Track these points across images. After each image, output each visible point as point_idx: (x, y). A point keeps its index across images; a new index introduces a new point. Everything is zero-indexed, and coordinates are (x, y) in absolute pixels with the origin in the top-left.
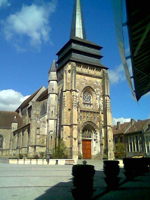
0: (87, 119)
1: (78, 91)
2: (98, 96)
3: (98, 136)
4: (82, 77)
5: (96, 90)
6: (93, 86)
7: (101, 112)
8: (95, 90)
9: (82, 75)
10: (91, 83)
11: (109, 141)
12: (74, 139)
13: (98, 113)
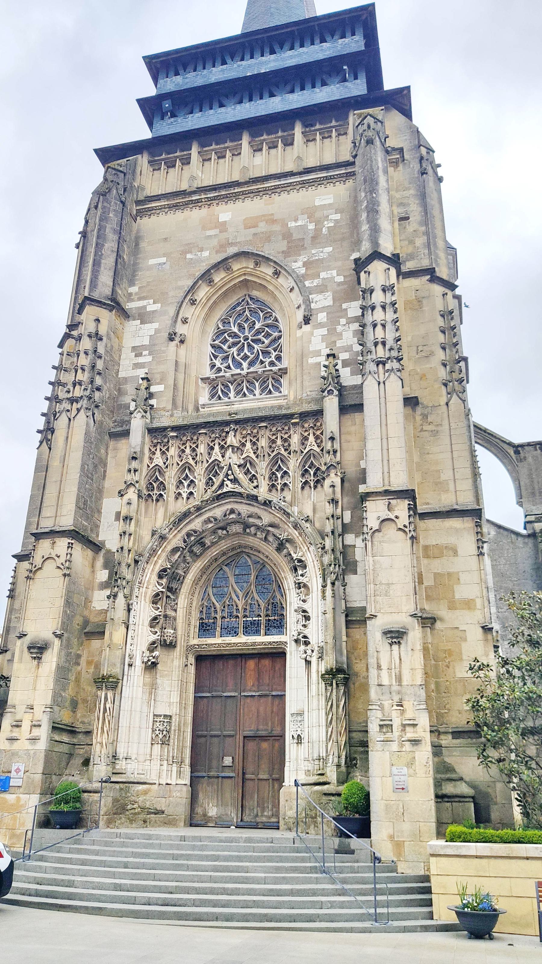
0: (209, 482)
1: (157, 306)
10: (262, 227)
13: (319, 413)
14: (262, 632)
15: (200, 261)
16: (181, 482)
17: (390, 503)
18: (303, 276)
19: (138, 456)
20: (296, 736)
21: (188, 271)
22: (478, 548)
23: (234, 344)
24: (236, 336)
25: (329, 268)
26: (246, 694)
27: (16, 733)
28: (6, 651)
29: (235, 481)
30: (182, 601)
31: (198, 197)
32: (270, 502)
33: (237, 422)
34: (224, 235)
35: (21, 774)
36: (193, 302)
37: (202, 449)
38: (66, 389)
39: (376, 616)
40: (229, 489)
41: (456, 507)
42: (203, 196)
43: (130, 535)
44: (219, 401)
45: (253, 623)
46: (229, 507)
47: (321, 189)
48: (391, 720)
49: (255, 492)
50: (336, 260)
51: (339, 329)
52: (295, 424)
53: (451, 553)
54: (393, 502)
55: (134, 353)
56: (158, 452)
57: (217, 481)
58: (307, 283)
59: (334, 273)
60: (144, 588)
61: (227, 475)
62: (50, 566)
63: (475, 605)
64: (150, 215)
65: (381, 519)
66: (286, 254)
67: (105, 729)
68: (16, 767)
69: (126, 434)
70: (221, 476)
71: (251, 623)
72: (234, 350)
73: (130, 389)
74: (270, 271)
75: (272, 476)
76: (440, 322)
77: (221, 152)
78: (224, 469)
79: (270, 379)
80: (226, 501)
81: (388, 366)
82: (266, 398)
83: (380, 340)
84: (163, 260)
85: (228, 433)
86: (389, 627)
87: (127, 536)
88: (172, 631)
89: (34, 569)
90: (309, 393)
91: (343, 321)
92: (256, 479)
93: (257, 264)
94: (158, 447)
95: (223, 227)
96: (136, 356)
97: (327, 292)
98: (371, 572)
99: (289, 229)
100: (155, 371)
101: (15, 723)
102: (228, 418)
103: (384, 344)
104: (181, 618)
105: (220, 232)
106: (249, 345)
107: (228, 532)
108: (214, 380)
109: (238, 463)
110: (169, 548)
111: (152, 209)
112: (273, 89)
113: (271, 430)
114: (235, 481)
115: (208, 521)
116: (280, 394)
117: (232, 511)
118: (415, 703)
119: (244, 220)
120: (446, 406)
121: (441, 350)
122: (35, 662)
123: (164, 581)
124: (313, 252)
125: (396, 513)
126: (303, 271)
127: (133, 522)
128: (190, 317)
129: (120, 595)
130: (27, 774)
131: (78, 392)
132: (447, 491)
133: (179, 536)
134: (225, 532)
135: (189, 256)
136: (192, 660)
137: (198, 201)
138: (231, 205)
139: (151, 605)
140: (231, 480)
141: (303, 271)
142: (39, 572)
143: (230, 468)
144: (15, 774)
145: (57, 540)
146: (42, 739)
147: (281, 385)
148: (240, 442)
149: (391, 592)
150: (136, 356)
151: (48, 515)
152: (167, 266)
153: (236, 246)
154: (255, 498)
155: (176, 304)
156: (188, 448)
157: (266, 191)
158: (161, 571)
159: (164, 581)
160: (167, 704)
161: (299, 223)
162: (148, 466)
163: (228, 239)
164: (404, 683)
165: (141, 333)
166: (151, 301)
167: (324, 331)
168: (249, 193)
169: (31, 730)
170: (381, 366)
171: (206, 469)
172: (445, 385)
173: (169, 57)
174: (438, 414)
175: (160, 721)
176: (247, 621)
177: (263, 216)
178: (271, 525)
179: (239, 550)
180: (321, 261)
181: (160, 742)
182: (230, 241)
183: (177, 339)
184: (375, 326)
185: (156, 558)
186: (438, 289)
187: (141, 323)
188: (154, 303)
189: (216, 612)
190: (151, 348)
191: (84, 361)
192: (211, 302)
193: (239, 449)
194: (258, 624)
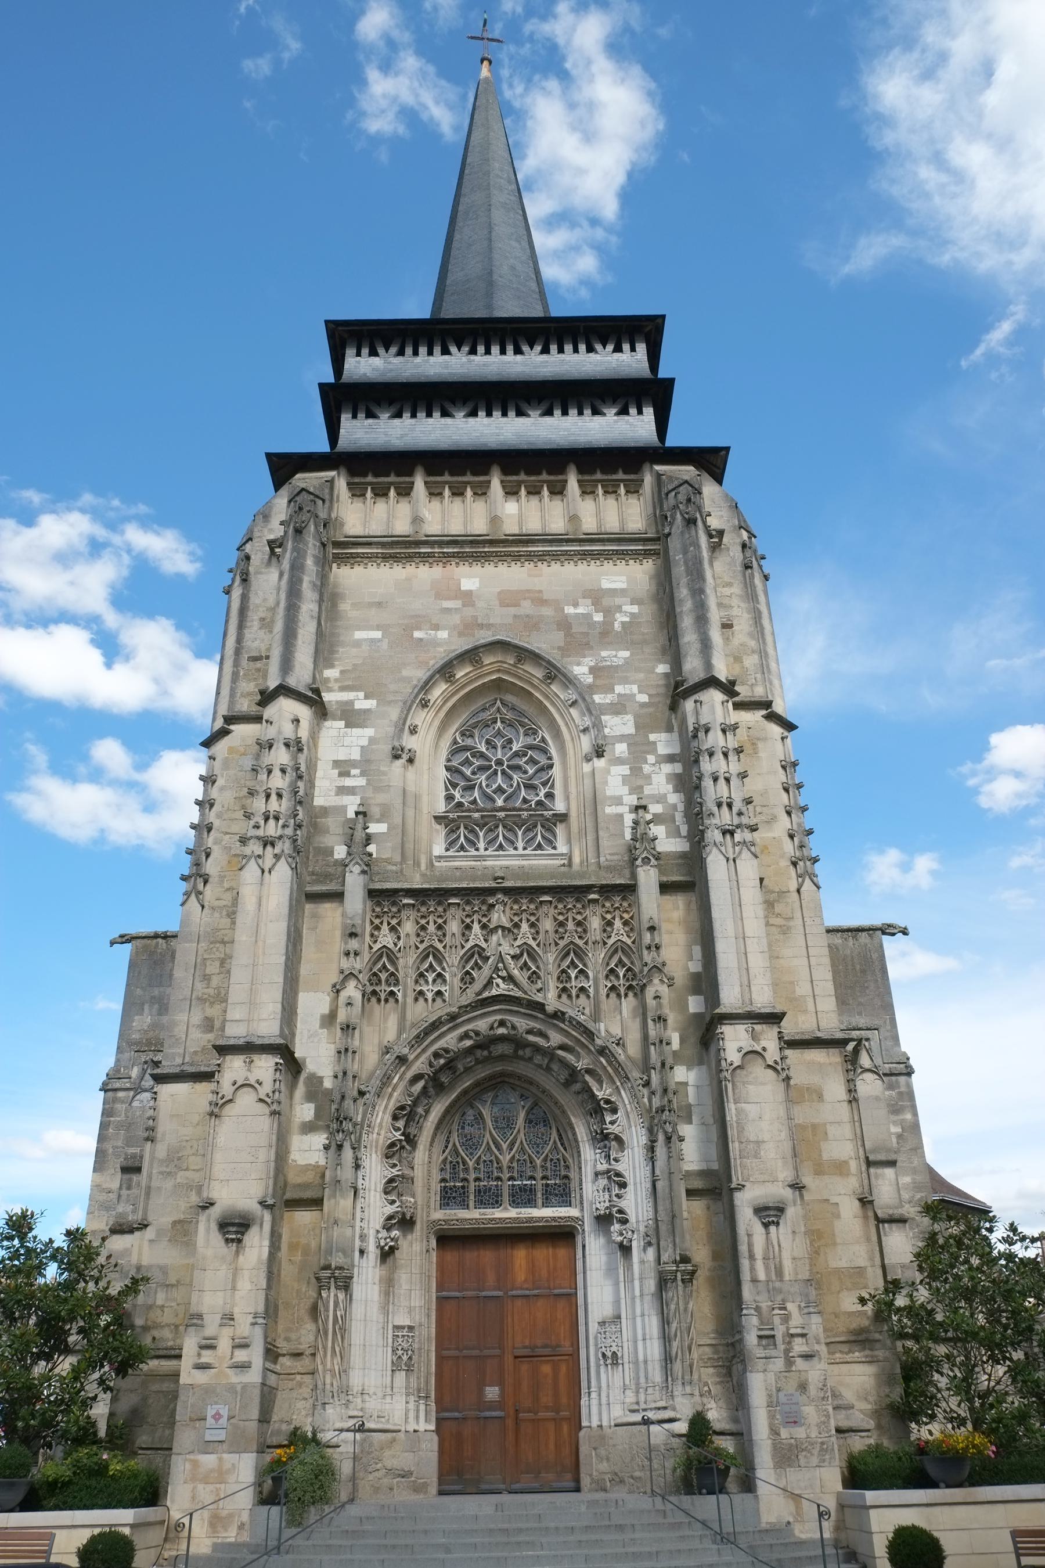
0: (467, 979)
1: (370, 704)
2: (620, 725)
3: (629, 1178)
4: (425, 574)
5: (593, 670)
6: (558, 638)
7: (648, 878)
8: (581, 670)
9: (425, 558)
10: (527, 607)
11: (760, 1211)
12: (223, 1226)
13: (629, 890)
14: (540, 1202)
15: (435, 643)
16: (421, 975)
17: (753, 1029)
18: (590, 687)
19: (359, 931)
20: (609, 1354)
21: (416, 657)
22: (850, 1091)
23: (482, 769)
24: (482, 755)
25: (625, 681)
26: (514, 1293)
27: (207, 1357)
28: (146, 1226)
29: (510, 979)
30: (420, 1155)
31: (429, 550)
32: (563, 1013)
33: (508, 891)
34: (469, 612)
35: (223, 1421)
36: (425, 704)
37: (454, 927)
38: (252, 823)
39: (744, 1186)
40: (500, 992)
41: (819, 1034)
42: (437, 550)
43: (354, 1052)
44: (462, 853)
45: (523, 1189)
46: (499, 1017)
47: (608, 566)
48: (772, 1329)
49: (539, 998)
50: (638, 670)
51: (647, 769)
52: (595, 901)
53: (815, 1096)
54: (758, 1027)
55: (336, 771)
56: (385, 928)
57: (481, 977)
58: (597, 698)
59: (635, 688)
60: (375, 1135)
61: (497, 969)
62: (246, 1100)
63: (849, 1170)
64: (353, 564)
65: (744, 1052)
66: (564, 651)
67: (337, 1349)
68: (214, 1412)
69: (338, 896)
70: (486, 970)
71: (520, 1189)
72: (482, 778)
73: (333, 824)
74: (539, 673)
75: (563, 976)
76: (782, 776)
77: (458, 488)
78: (490, 960)
79: (539, 827)
80: (492, 1009)
81: (738, 837)
82: (535, 855)
83: (724, 800)
84: (377, 634)
85: (492, 906)
86: (761, 1202)
87: (350, 1054)
88: (412, 1200)
89: (221, 1102)
90: (608, 857)
91: (651, 759)
92: (539, 977)
93: (520, 661)
94: (385, 919)
95: (468, 598)
96: (341, 775)
97: (626, 713)
98: (735, 1125)
99: (566, 616)
100: (373, 801)
101: (204, 1342)
102: (493, 884)
103: (730, 806)
104: (420, 1180)
105: (464, 606)
106: (504, 772)
107: (490, 1053)
108: (453, 820)
109: (512, 953)
110: (409, 1075)
111: (358, 555)
112: (524, 406)
113: (556, 907)
114: (510, 979)
115: (466, 1036)
116: (553, 852)
117: (502, 1023)
118: (803, 1305)
119: (499, 593)
120: (796, 894)
121: (785, 815)
122: (234, 1246)
123: (401, 1124)
124: (604, 654)
125: (763, 1043)
126: (590, 680)
127: (357, 1032)
128: (420, 724)
129: (347, 1146)
130: (232, 1421)
131: (272, 829)
132: (805, 1011)
133: (423, 1058)
134: (485, 1053)
135: (417, 634)
136: (433, 1243)
137: (429, 555)
138: (477, 568)
139: (385, 1160)
140: (503, 978)
141: (590, 680)
142: (228, 1107)
143: (501, 959)
144: (213, 1421)
145: (255, 1057)
146: (253, 1366)
147: (555, 836)
148: (512, 920)
149: (762, 1153)
150: (341, 775)
151: (237, 1017)
152: (385, 645)
153: (489, 629)
154: (540, 1007)
155: (401, 704)
156: (431, 923)
157: (530, 557)
158: (397, 1109)
159: (401, 1124)
160: (406, 1310)
161: (581, 610)
162: (371, 948)
163: (475, 618)
164: (787, 1278)
165: (347, 741)
166: (361, 695)
167: (625, 770)
168: (505, 555)
169: (232, 1353)
170: (728, 837)
171: (462, 958)
172: (795, 864)
173: (365, 328)
174: (787, 903)
175: (403, 1336)
176: (513, 1185)
177: (528, 591)
178: (563, 1047)
179: (499, 1080)
180: (616, 668)
181: (404, 1367)
182: (479, 621)
183: (405, 757)
184: (715, 779)
185: (390, 1089)
186: (776, 730)
187: (347, 726)
188: (366, 697)
189: (466, 1170)
190: (366, 764)
191: (278, 781)
192: (450, 704)
193: (511, 931)
194: (532, 1190)
